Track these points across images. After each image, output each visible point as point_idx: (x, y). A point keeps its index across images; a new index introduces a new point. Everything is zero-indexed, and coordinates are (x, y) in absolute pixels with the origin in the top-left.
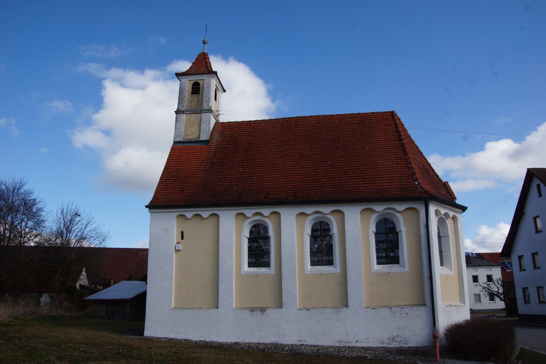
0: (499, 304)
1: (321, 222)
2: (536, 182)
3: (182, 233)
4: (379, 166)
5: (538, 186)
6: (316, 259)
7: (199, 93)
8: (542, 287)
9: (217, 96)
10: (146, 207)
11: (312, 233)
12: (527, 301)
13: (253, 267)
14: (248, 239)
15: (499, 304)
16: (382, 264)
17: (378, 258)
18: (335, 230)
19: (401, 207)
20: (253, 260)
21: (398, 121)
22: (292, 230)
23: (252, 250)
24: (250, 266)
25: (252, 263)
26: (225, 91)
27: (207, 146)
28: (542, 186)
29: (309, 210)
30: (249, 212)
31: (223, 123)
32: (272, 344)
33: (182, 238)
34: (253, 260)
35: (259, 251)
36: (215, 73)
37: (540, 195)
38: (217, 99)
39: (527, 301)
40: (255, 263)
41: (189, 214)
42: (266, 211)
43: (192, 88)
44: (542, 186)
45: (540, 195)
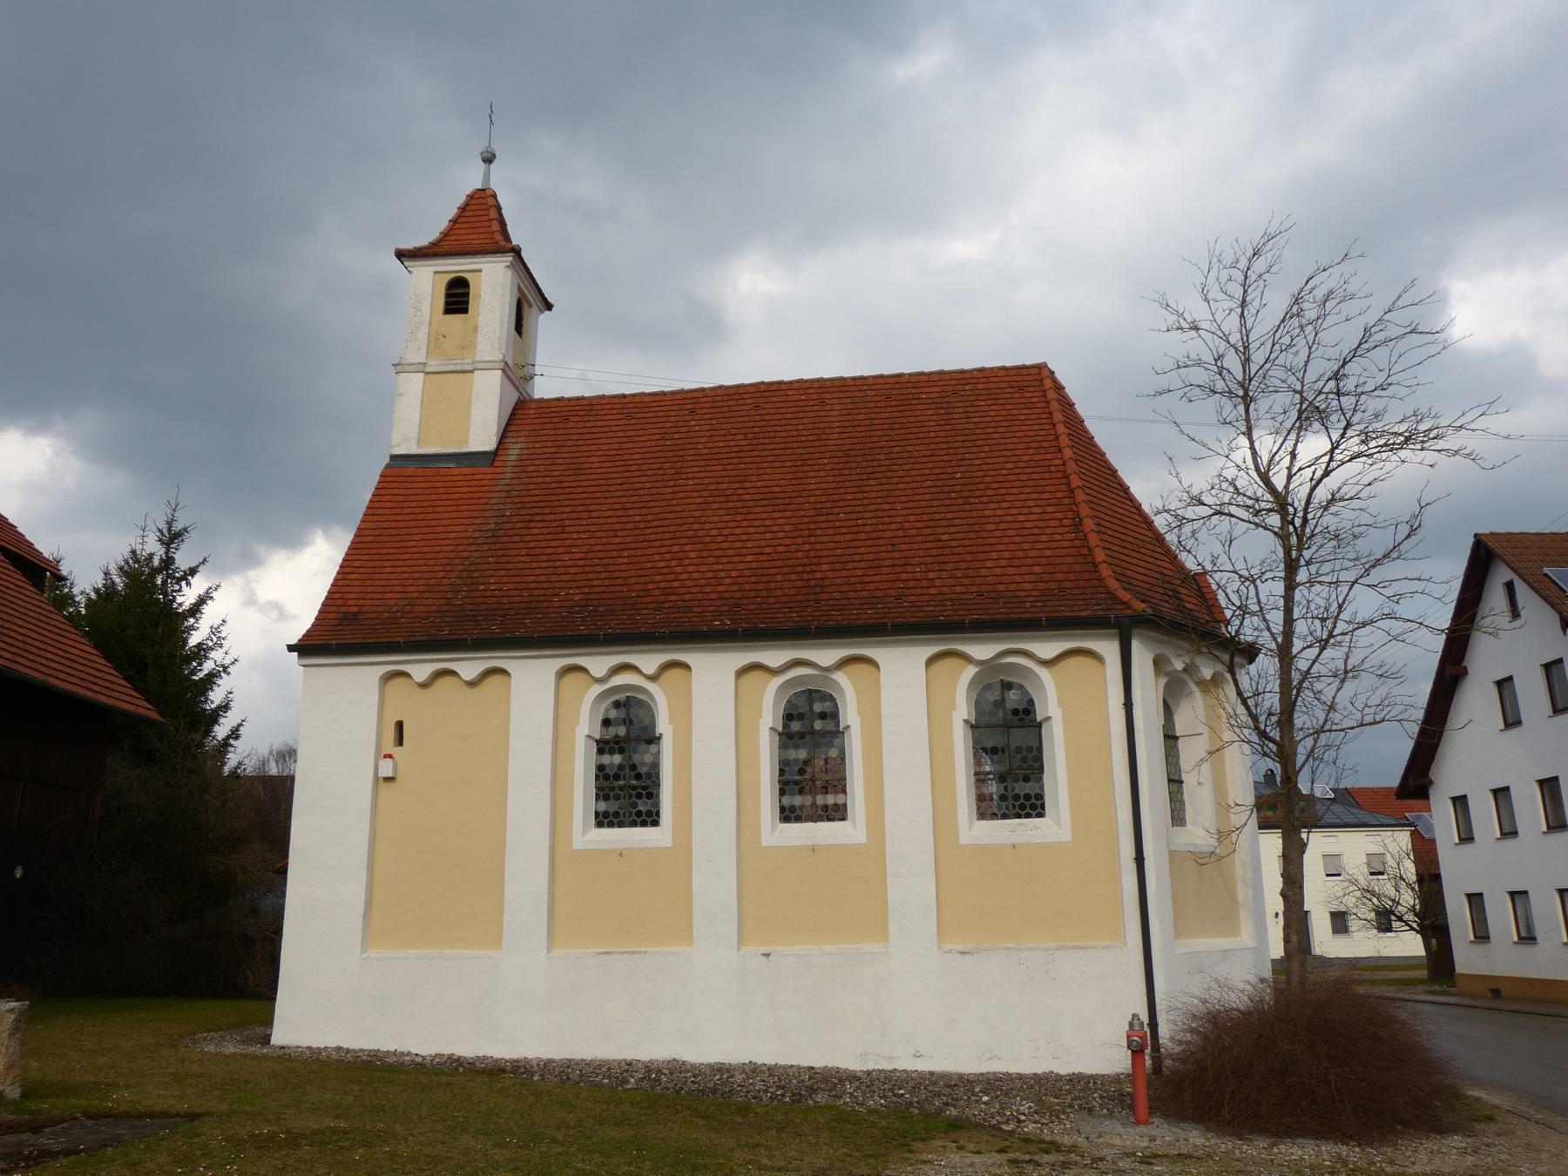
0: (1408, 944)
1: (813, 695)
2: (1500, 575)
3: (400, 726)
4: (990, 527)
5: (1510, 586)
6: (798, 800)
7: (465, 311)
8: (1526, 892)
9: (524, 323)
10: (291, 648)
11: (785, 726)
12: (1482, 935)
13: (611, 825)
14: (598, 742)
15: (1408, 944)
16: (994, 816)
17: (981, 798)
18: (851, 715)
19: (1047, 648)
20: (611, 806)
21: (1052, 395)
22: (715, 709)
23: (607, 777)
24: (603, 820)
25: (606, 814)
26: (549, 307)
27: (489, 470)
28: (1522, 590)
29: (775, 656)
30: (598, 663)
31: (542, 400)
32: (742, 1068)
33: (400, 741)
34: (611, 806)
35: (627, 784)
36: (517, 252)
37: (1515, 614)
38: (524, 330)
39: (1482, 935)
40: (616, 814)
41: (421, 669)
42: (649, 661)
43: (448, 296)
44: (1522, 590)
45: (1515, 614)
